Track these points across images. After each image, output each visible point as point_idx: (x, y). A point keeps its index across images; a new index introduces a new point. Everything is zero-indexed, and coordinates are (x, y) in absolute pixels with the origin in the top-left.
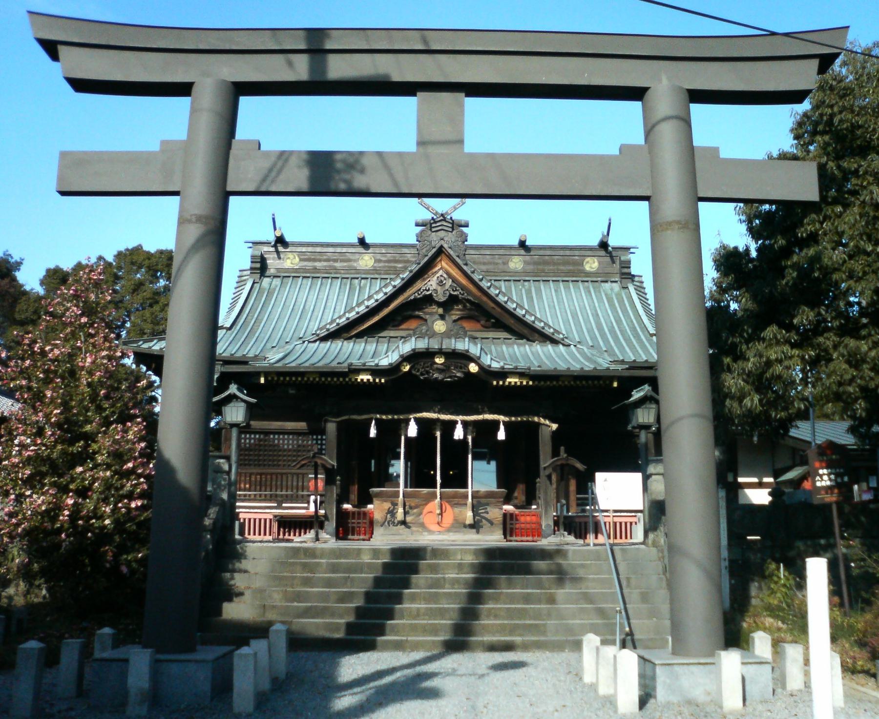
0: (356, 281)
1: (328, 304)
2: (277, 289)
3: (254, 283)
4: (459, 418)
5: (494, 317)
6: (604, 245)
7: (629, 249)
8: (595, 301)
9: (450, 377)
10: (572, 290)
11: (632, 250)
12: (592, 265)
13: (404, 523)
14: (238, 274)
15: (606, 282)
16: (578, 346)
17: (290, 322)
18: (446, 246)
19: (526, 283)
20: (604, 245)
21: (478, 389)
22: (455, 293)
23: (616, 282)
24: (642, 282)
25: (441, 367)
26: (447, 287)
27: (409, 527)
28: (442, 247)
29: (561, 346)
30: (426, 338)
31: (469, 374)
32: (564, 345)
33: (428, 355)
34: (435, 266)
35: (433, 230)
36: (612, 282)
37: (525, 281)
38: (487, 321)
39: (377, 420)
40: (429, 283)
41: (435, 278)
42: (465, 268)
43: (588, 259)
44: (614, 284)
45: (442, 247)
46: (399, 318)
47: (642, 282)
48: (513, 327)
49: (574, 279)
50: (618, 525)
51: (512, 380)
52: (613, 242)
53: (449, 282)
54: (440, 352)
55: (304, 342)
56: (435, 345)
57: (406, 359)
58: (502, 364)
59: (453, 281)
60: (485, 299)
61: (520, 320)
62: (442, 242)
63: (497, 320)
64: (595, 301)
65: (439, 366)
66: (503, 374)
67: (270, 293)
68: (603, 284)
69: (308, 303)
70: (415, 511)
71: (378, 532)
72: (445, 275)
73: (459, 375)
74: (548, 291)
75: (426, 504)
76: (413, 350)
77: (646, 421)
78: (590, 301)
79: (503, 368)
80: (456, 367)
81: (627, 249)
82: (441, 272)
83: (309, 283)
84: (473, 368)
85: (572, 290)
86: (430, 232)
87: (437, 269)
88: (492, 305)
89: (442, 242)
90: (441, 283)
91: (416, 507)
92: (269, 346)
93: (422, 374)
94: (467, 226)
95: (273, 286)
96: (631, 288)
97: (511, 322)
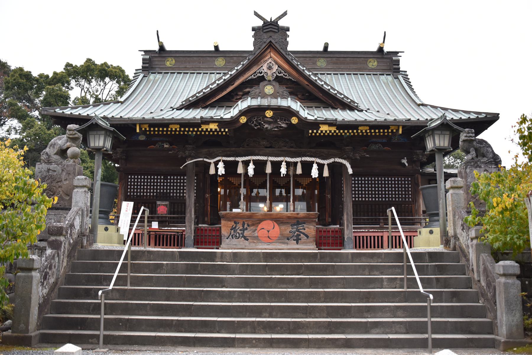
0: (213, 75)
1: (193, 88)
2: (160, 80)
3: (144, 76)
4: (298, 160)
5: (308, 92)
6: (381, 49)
7: (398, 53)
8: (377, 86)
9: (277, 127)
10: (360, 79)
11: (400, 54)
12: (373, 63)
13: (399, 126)
14: (135, 72)
15: (383, 75)
16: (368, 111)
17: (166, 99)
18: (273, 41)
19: (329, 76)
20: (381, 49)
21: (301, 138)
22: (280, 75)
23: (390, 75)
24: (407, 75)
25: (271, 120)
26: (274, 70)
27: (247, 240)
28: (270, 42)
29: (356, 111)
30: (259, 98)
31: (291, 125)
32: (358, 111)
33: (260, 110)
34: (266, 56)
35: (265, 31)
36: (387, 75)
37: (328, 74)
38: (303, 95)
39: (302, 162)
40: (262, 68)
41: (266, 64)
42: (287, 57)
43: (371, 59)
44: (389, 76)
45: (270, 42)
46: (241, 93)
47: (407, 75)
48: (321, 98)
49: (361, 73)
50: (376, 238)
51: (324, 128)
52: (386, 49)
53: (275, 68)
54: (269, 108)
55: (173, 109)
56: (265, 102)
57: (243, 113)
58: (316, 117)
59: (278, 67)
60: (301, 79)
61: (326, 93)
62: (271, 39)
63: (310, 94)
64: (377, 86)
65: (268, 119)
66: (316, 124)
67: (154, 82)
68: (381, 76)
69: (179, 88)
70: (252, 228)
71: (225, 242)
72: (273, 62)
73: (283, 125)
74: (344, 80)
75: (260, 223)
76: (249, 106)
77: (97, 145)
78: (373, 86)
79: (316, 119)
80: (281, 120)
81: (396, 53)
82: (270, 61)
83: (181, 77)
84: (294, 120)
85: (360, 79)
86: (262, 33)
87: (267, 58)
88: (306, 83)
89: (271, 39)
90: (270, 68)
91: (253, 225)
92: (270, 241)
93: (256, 125)
94: (289, 30)
95: (157, 78)
96: (400, 77)
97: (320, 95)
